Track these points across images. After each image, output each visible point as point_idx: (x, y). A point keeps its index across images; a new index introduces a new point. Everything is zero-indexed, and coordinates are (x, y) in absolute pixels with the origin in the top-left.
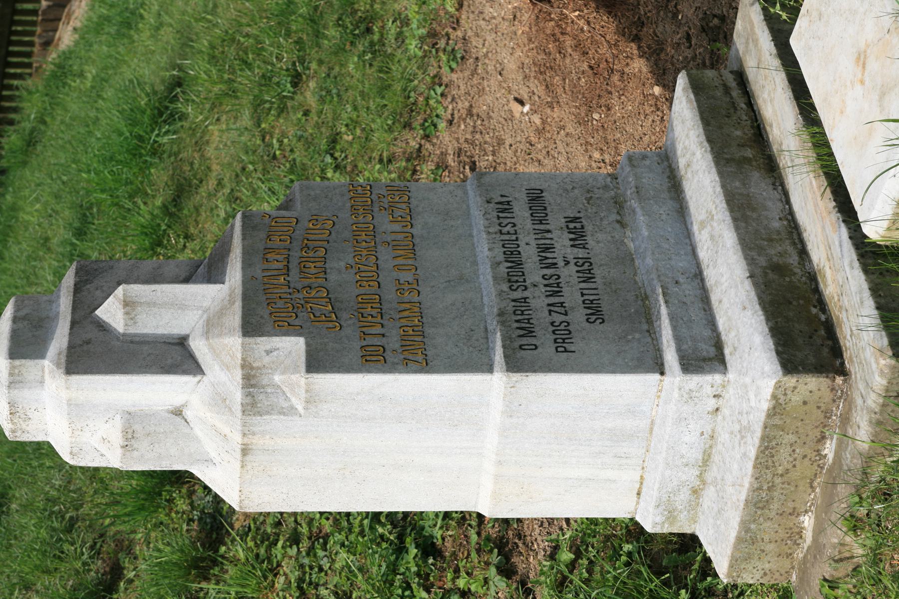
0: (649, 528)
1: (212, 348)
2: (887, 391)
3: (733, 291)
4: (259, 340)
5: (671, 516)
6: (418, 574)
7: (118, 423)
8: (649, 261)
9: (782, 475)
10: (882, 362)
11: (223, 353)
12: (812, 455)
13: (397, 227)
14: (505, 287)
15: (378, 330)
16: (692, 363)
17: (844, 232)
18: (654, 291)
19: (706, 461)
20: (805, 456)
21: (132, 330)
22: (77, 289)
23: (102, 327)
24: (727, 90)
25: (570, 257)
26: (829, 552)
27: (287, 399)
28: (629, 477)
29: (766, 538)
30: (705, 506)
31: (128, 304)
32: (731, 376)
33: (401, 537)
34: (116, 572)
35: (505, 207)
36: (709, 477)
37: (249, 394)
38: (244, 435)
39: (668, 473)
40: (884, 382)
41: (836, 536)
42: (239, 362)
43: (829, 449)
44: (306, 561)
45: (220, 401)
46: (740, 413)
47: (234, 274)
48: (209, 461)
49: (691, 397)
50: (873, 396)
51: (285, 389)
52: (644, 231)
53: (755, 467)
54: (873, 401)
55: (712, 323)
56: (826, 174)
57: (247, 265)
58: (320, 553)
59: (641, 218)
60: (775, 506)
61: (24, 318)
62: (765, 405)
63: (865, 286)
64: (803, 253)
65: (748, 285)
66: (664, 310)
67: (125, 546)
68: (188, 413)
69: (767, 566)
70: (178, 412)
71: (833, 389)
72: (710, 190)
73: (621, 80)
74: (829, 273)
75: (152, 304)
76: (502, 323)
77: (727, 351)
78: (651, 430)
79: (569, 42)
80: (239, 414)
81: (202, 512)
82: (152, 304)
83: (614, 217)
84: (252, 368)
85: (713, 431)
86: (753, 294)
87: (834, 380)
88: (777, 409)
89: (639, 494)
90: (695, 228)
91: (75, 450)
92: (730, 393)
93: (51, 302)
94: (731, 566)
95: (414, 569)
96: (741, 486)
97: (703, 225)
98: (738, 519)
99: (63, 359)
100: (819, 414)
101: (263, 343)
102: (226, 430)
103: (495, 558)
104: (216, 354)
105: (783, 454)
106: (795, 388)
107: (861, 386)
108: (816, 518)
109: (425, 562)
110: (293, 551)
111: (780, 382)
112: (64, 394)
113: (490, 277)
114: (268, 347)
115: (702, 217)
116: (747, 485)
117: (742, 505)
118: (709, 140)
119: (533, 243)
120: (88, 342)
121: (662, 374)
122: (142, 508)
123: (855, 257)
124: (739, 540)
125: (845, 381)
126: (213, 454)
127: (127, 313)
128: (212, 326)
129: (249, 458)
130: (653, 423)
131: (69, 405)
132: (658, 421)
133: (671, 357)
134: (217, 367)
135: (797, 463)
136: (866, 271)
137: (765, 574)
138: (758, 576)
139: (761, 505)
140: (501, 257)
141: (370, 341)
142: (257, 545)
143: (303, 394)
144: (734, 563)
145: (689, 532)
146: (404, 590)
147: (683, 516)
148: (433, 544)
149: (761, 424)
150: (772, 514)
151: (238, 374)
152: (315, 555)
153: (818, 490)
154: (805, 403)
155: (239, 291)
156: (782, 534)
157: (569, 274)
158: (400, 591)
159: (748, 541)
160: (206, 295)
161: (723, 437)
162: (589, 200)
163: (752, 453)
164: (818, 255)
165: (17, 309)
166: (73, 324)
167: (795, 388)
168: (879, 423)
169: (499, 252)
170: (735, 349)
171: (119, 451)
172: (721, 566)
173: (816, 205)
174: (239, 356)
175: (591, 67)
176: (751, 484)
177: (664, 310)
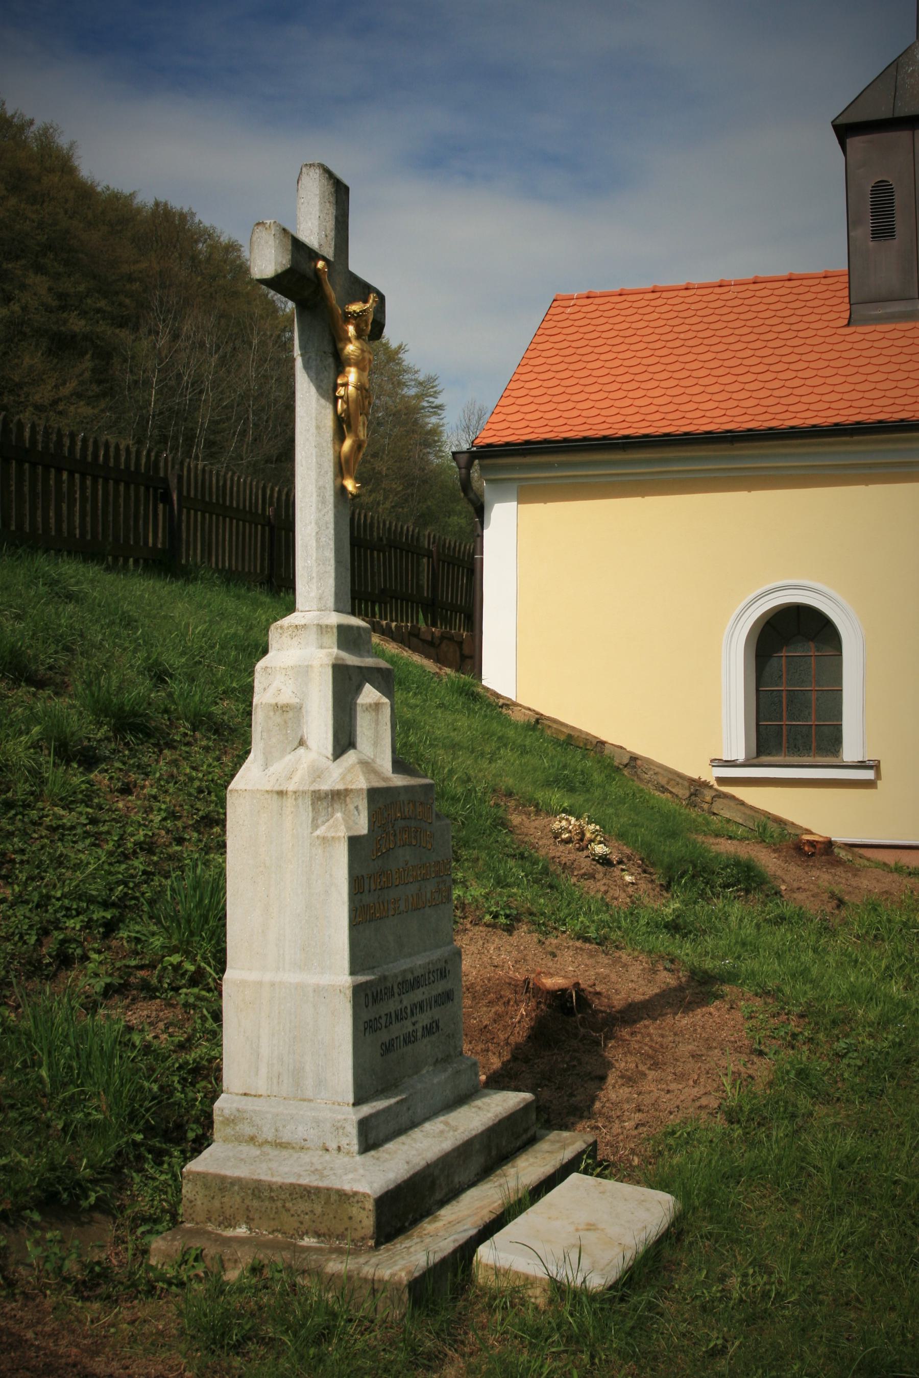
0: (217, 1105)
1: (353, 766)
2: (379, 1281)
3: (414, 1152)
4: (365, 801)
5: (230, 1121)
6: (90, 920)
7: (294, 701)
8: (419, 1086)
9: (284, 1206)
10: (403, 1274)
11: (347, 774)
12: (303, 1228)
13: (429, 895)
14: (400, 979)
15: (373, 887)
16: (364, 1125)
17: (473, 1232)
18: (402, 1092)
19: (281, 1145)
20: (301, 1223)
21: (359, 709)
22: (379, 670)
23: (359, 689)
24: (526, 1130)
25: (417, 1026)
26: (227, 1251)
27: (324, 823)
28: (261, 1086)
29: (225, 1200)
30: (240, 1148)
31: (377, 706)
32: (358, 1158)
33: (114, 905)
34: (41, 684)
35: (443, 974)
36: (267, 1148)
37: (327, 794)
38: (295, 792)
39: (269, 1116)
40: (386, 1278)
41: (246, 1258)
42: (350, 787)
43: (309, 1241)
44: (79, 831)
45: (317, 774)
46: (332, 1169)
47: (399, 781)
48: (266, 766)
49: (338, 1128)
50: (372, 1271)
51: (331, 821)
52: (435, 1081)
53: (291, 1184)
54: (368, 1271)
55: (388, 1139)
56: (503, 1213)
57: (406, 788)
58: (88, 842)
59: (443, 1076)
60: (255, 1203)
61: (360, 635)
62: (347, 1187)
63: (445, 1253)
64: (443, 1203)
65: (423, 1163)
66: (393, 1101)
67: (60, 690)
68: (301, 750)
69: (199, 1203)
70: (302, 743)
71: (363, 1239)
72: (471, 1127)
73: (482, 1051)
74: (439, 1224)
75: (377, 722)
76: (380, 980)
77: (373, 1153)
78: (304, 1100)
79: (500, 1008)
80: (312, 788)
81: (96, 749)
82: (377, 722)
83: (440, 1056)
84: (346, 796)
85: (308, 1149)
86: (418, 1168)
87: (371, 1238)
88: (344, 1197)
89: (245, 1094)
90: (442, 1118)
91: (269, 671)
92: (343, 1159)
93: (368, 652)
94: (198, 1174)
95: (95, 917)
96: (272, 1176)
97: (447, 1124)
98: (242, 1175)
99: (340, 662)
100: (341, 1229)
101: (363, 805)
102: (296, 778)
103: (117, 981)
104: (350, 770)
105: (303, 1206)
106: (364, 1209)
107: (374, 1260)
108: (247, 1238)
109: (100, 926)
110: (83, 820)
111: (369, 1196)
112: (316, 663)
113: (404, 967)
114: (360, 807)
115: (450, 1121)
116: (274, 1179)
117: (255, 1177)
118: (500, 1121)
119: (424, 997)
120: (350, 679)
121: (354, 1105)
122: (97, 701)
123: (461, 1242)
124: (223, 1178)
125: (371, 1247)
126: (271, 769)
127: (370, 705)
128: (367, 766)
129: (275, 796)
130: (310, 1101)
131: (307, 666)
132: (312, 1105)
133: (366, 1110)
134: (341, 771)
135: (296, 1218)
136: (455, 1252)
137: (191, 1202)
138: (189, 1196)
139: (256, 1192)
140: (416, 974)
141: (367, 881)
142: (82, 792)
143: (330, 834)
144: (202, 1177)
145: (215, 1137)
146: (76, 910)
147: (229, 1131)
148: (113, 931)
149: (330, 1186)
150: (247, 1202)
151: (340, 787)
152: (85, 838)
153: (271, 1236)
154: (350, 1218)
155: (391, 784)
156: (228, 1213)
157: (407, 1026)
158: (75, 906)
159: (221, 1185)
160: (385, 763)
161: (306, 1157)
162: (448, 1036)
163: (304, 1181)
164: (447, 1213)
165: (364, 629)
166: (359, 668)
167: (364, 1209)
168: (349, 1278)
169: (418, 973)
170: (378, 1159)
171: (273, 702)
172: (195, 1166)
173: (482, 1208)
174: (353, 787)
175: (486, 1027)
176: (276, 1183)
177: (393, 1101)
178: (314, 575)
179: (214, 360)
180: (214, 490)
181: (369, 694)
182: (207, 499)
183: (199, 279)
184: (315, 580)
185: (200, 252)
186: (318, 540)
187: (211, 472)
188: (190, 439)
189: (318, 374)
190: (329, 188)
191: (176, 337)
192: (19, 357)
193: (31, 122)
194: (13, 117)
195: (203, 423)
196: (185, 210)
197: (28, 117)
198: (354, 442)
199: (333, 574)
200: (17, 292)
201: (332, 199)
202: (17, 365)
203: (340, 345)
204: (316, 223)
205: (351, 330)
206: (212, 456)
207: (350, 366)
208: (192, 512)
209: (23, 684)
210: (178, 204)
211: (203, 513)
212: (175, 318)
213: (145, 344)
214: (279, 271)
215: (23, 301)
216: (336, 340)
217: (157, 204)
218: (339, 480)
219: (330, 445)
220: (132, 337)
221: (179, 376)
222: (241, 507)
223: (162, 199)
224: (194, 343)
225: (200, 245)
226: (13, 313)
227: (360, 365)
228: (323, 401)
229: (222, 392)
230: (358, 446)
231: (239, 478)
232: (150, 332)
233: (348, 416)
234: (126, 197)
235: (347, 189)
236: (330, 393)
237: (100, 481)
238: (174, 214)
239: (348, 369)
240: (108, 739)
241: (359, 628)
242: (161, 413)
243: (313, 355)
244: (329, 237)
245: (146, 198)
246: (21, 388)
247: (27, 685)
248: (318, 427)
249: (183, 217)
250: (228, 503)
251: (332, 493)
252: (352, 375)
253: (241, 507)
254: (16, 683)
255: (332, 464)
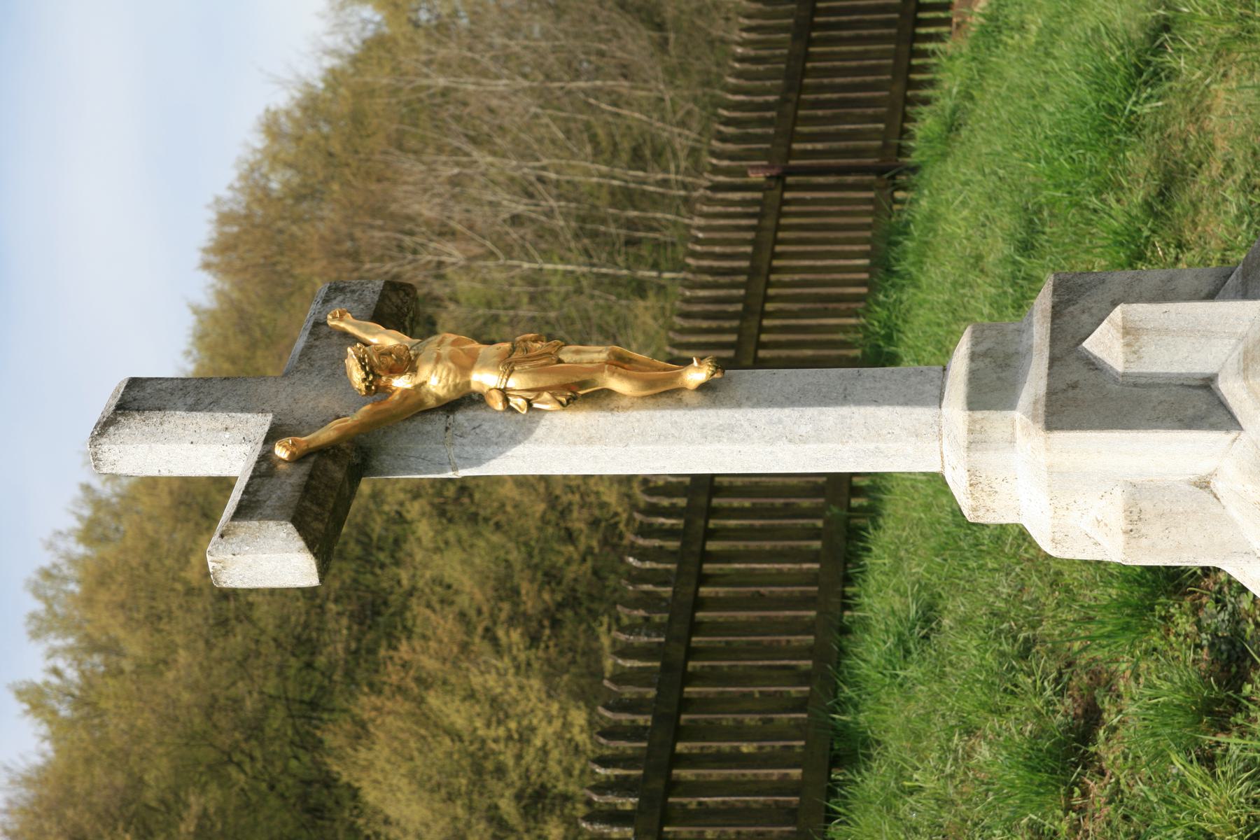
7: (1118, 499)
21: (1135, 369)
23: (1093, 364)
31: (1129, 331)
34: (1092, 716)
61: (985, 354)
68: (1218, 486)
70: (1203, 484)
75: (1163, 331)
81: (1215, 635)
82: (1163, 331)
99: (1041, 410)
122: (1126, 628)
127: (1128, 345)
131: (1050, 473)
166: (1053, 361)
171: (1121, 538)
178: (872, 446)
179: (483, 158)
180: (722, 293)
181: (1105, 343)
182: (739, 307)
183: (335, 187)
184: (882, 446)
185: (286, 184)
186: (803, 440)
187: (688, 301)
188: (627, 197)
189: (487, 442)
190: (134, 425)
191: (446, 233)
192: (503, 505)
193: (87, 488)
194: (80, 518)
195: (602, 175)
196: (212, 215)
197: (78, 493)
198: (613, 373)
199: (869, 411)
200: (386, 508)
201: (156, 416)
202: (516, 506)
203: (431, 402)
204: (203, 448)
205: (401, 383)
206: (658, 154)
207: (468, 383)
208: (764, 337)
209: (1092, 749)
210: (202, 230)
211: (765, 315)
212: (411, 233)
213: (463, 284)
214: (302, 544)
215: (402, 496)
216: (419, 410)
217: (207, 266)
218: (687, 397)
219: (621, 416)
220: (452, 306)
221: (516, 220)
222: (750, 235)
223: (197, 258)
224: (454, 196)
225: (275, 185)
226: (423, 514)
227: (465, 365)
228: (540, 432)
229: (540, 141)
230: (620, 363)
231: (698, 241)
232: (440, 277)
233: (566, 387)
234: (201, 322)
235: (134, 383)
236: (522, 422)
237: (716, 502)
238: (221, 234)
239: (474, 387)
240: (1197, 609)
241: (973, 357)
242: (587, 252)
243: (453, 451)
244: (228, 422)
245: (202, 288)
246: (557, 497)
247: (1094, 742)
248: (589, 441)
249: (225, 219)
250: (745, 264)
251: (712, 412)
252: (485, 379)
253: (750, 235)
254: (1089, 762)
255: (658, 414)
